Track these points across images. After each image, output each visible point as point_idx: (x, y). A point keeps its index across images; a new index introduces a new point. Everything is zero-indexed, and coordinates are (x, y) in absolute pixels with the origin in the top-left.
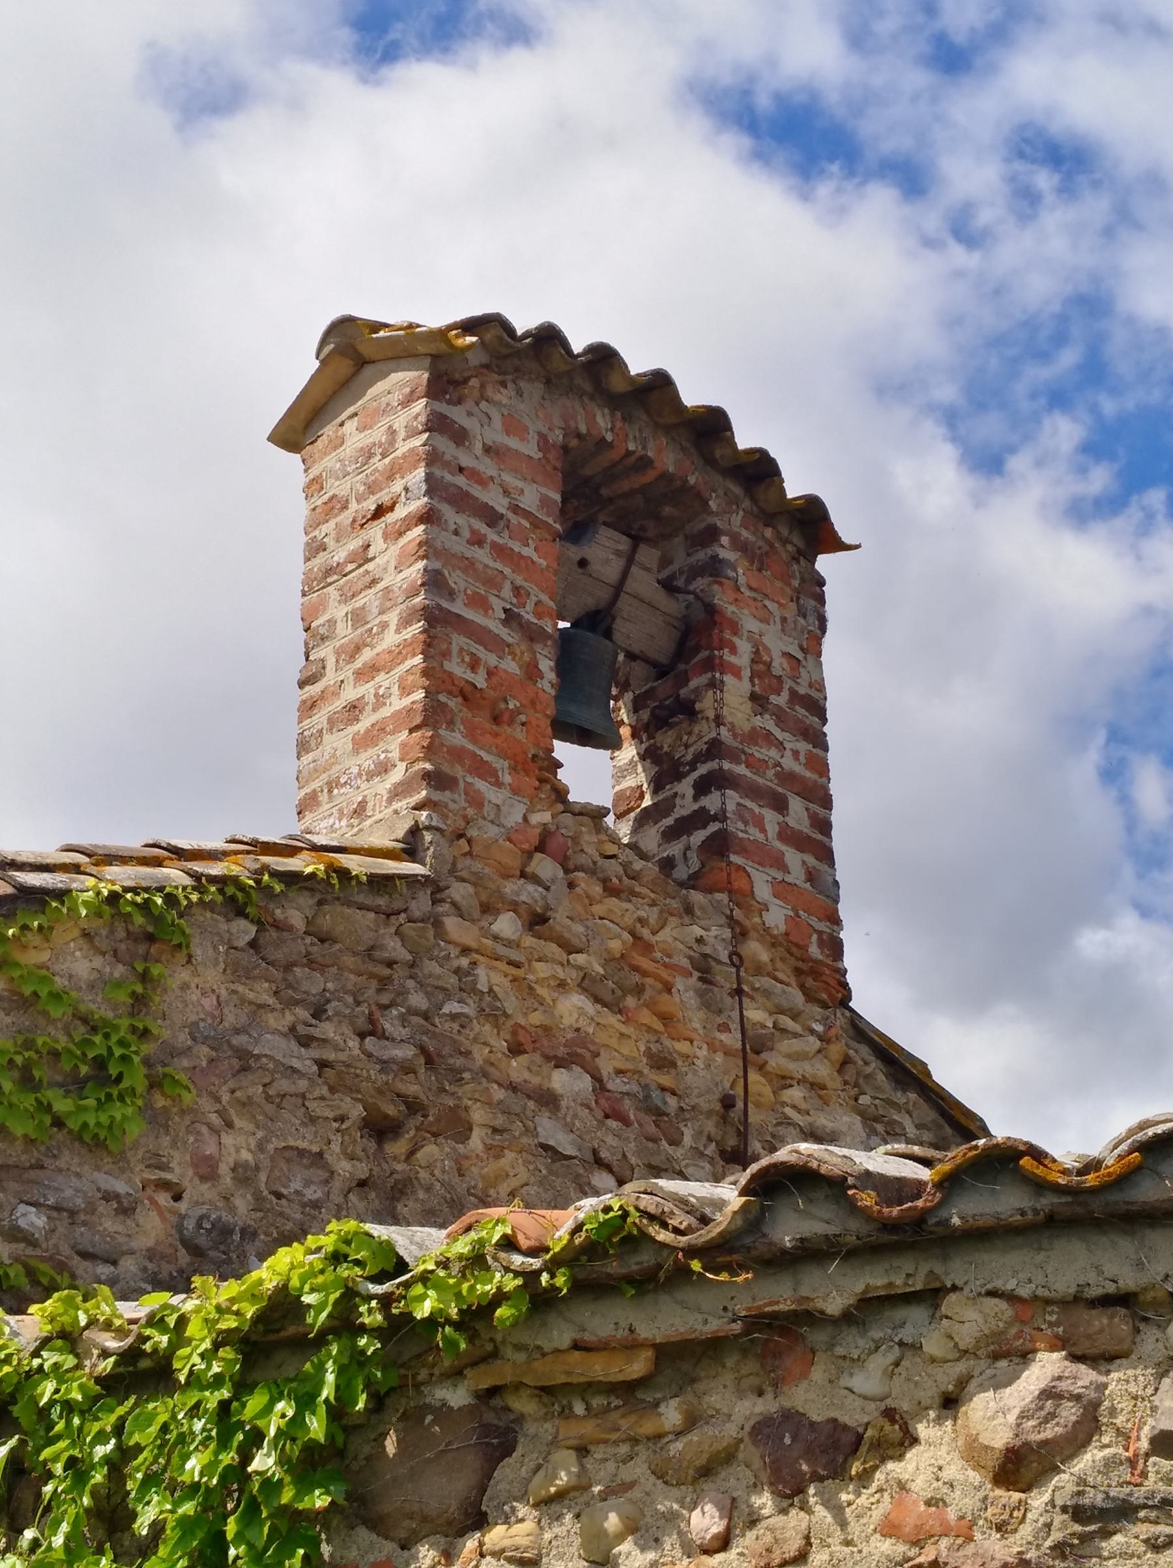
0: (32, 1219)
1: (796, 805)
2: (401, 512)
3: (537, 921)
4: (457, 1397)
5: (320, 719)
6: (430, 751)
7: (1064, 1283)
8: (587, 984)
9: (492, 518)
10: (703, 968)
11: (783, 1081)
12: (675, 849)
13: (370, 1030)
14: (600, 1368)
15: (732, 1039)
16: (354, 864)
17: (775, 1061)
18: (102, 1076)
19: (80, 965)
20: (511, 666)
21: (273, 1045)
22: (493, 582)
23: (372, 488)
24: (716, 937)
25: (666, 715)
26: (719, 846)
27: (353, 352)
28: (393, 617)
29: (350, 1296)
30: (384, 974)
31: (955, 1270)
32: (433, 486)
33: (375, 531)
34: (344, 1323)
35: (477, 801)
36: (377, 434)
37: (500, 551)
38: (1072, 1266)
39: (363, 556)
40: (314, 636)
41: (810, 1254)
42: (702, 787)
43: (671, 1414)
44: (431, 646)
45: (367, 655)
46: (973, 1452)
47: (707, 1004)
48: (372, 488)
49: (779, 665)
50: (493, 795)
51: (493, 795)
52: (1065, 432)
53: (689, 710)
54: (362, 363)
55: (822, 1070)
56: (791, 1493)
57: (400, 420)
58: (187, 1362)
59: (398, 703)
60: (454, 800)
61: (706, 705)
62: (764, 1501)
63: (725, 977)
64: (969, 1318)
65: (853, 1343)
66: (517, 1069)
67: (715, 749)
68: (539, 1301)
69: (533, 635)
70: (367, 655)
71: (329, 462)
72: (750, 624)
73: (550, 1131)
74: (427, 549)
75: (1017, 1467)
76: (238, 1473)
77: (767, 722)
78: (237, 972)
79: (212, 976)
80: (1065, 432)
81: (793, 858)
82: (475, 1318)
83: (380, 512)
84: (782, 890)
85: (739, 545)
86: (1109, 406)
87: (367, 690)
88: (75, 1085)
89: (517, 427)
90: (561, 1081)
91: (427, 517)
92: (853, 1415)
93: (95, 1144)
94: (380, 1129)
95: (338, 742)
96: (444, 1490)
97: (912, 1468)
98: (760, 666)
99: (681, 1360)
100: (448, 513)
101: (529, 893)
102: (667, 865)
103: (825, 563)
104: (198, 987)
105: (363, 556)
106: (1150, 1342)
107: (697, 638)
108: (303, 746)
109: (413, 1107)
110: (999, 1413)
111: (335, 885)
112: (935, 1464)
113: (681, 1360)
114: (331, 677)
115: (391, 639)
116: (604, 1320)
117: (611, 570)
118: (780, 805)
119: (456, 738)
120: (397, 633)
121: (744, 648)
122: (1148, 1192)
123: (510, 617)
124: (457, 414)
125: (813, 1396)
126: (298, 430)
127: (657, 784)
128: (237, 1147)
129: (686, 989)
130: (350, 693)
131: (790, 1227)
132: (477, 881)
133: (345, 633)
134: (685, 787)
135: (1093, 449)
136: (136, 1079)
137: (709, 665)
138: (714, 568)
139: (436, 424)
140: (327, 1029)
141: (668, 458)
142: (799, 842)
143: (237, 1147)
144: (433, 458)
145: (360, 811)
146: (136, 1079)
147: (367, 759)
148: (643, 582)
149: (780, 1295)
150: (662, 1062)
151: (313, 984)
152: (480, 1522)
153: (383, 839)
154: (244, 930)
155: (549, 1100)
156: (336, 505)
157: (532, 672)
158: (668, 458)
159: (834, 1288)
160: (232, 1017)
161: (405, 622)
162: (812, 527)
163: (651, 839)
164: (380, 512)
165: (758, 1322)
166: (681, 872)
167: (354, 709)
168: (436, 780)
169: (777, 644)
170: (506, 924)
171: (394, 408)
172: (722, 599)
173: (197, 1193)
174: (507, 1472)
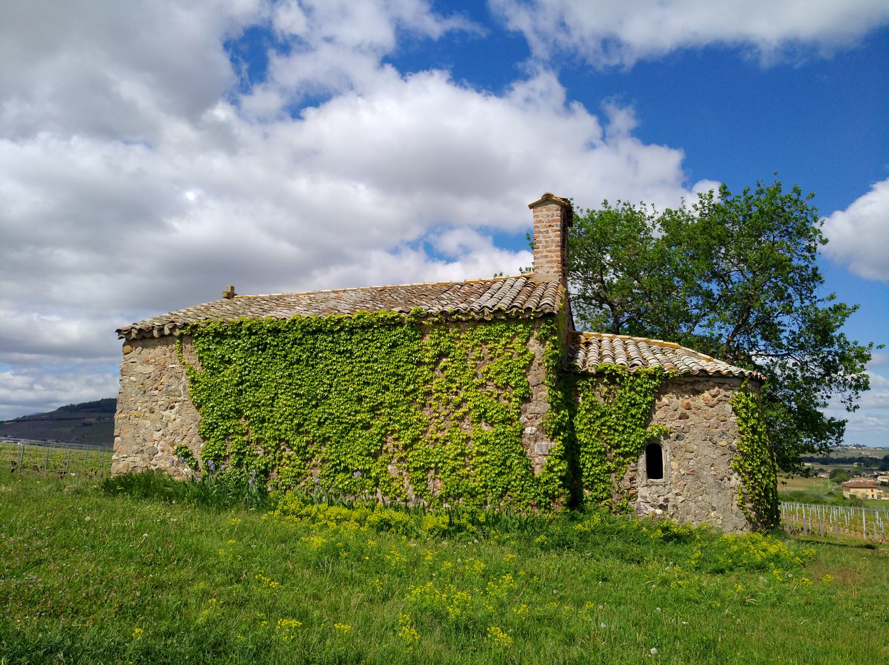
27: (547, 199)
33: (550, 229)
36: (550, 213)
64: (711, 383)
75: (714, 396)
87: (549, 254)
105: (547, 232)
112: (706, 394)
115: (553, 248)
125: (696, 387)
167: (546, 256)
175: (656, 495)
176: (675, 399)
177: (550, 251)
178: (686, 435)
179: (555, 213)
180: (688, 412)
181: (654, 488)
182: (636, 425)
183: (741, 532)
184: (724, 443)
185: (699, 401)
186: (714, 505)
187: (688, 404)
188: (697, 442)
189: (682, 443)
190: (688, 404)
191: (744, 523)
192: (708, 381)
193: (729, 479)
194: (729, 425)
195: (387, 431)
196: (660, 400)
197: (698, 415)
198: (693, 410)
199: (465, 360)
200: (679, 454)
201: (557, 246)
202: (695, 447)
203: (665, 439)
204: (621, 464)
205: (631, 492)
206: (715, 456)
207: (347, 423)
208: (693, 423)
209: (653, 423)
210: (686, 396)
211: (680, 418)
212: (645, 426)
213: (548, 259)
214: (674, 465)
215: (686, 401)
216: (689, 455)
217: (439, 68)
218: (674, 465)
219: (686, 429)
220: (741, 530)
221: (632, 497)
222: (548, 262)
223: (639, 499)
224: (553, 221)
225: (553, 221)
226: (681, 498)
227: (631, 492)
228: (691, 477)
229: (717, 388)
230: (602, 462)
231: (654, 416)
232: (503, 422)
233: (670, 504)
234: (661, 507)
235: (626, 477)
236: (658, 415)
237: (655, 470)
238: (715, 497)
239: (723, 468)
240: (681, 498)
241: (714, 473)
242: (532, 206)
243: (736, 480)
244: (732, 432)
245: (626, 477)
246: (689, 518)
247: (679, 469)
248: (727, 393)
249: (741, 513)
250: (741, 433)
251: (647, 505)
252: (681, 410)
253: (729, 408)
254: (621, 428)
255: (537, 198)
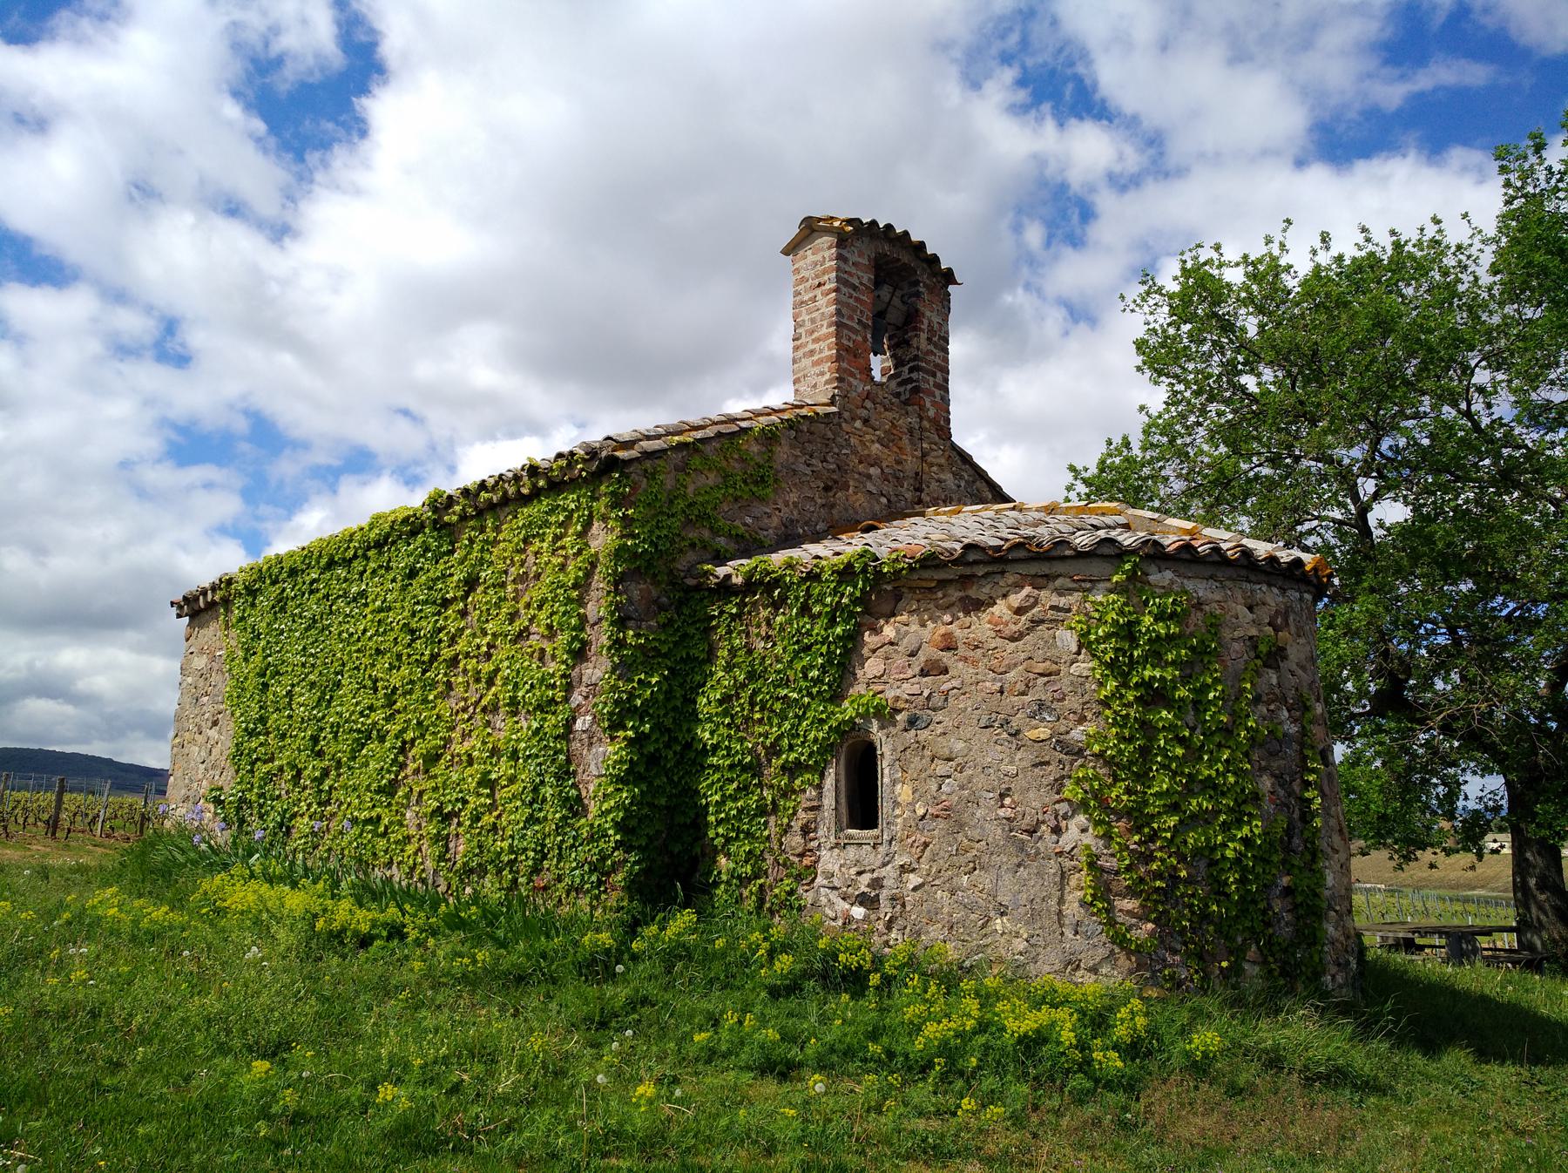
0: (749, 520)
1: (939, 374)
2: (827, 287)
3: (866, 421)
4: (889, 588)
5: (800, 353)
6: (838, 371)
7: (1033, 572)
8: (880, 441)
9: (855, 288)
10: (911, 431)
11: (932, 465)
12: (901, 389)
13: (824, 460)
14: (924, 584)
15: (918, 453)
16: (819, 410)
17: (929, 459)
18: (762, 481)
19: (755, 448)
20: (860, 338)
21: (802, 468)
22: (854, 311)
23: (817, 276)
24: (913, 420)
25: (900, 347)
26: (916, 390)
27: (811, 228)
28: (825, 323)
29: (866, 565)
30: (827, 443)
31: (1008, 568)
32: (838, 279)
33: (818, 292)
34: (864, 570)
35: (850, 385)
36: (818, 257)
37: (857, 299)
38: (1034, 568)
39: (814, 299)
40: (798, 325)
41: (976, 562)
42: (911, 370)
43: (940, 594)
44: (838, 335)
45: (816, 335)
46: (1010, 607)
47: (912, 443)
48: (817, 276)
49: (936, 326)
50: (855, 382)
51: (855, 382)
52: (1009, 75)
53: (907, 343)
54: (813, 231)
55: (943, 461)
56: (967, 613)
57: (827, 254)
58: (825, 577)
59: (827, 353)
60: (844, 386)
61: (914, 342)
62: (961, 615)
63: (917, 434)
64: (1011, 579)
65: (983, 582)
66: (861, 468)
67: (916, 358)
68: (911, 568)
69: (865, 326)
70: (816, 335)
71: (801, 263)
72: (928, 314)
73: (870, 487)
74: (837, 301)
75: (1019, 611)
76: (839, 603)
77: (931, 347)
78: (792, 447)
79: (786, 449)
80: (1009, 75)
81: (937, 393)
82: (897, 572)
83: (819, 285)
84: (934, 404)
85: (925, 286)
86: (1030, 62)
87: (816, 346)
88: (756, 483)
89: (861, 254)
90: (874, 471)
91: (837, 290)
92: (982, 597)
93: (762, 500)
94: (827, 489)
95: (807, 362)
96: (886, 608)
97: (995, 609)
98: (931, 330)
99: (943, 584)
100: (844, 290)
101: (864, 413)
102: (898, 395)
103: (951, 288)
104: (783, 452)
105: (814, 299)
106: (1051, 585)
107: (912, 318)
108: (794, 361)
109: (836, 482)
110: (1016, 599)
111: (815, 419)
112: (1000, 609)
113: (943, 584)
114: (803, 340)
115: (824, 330)
116: (927, 574)
117: (887, 299)
118: (934, 375)
119: (845, 365)
120: (826, 329)
121: (926, 322)
122: (1054, 553)
123: (860, 322)
124: (844, 252)
125: (973, 593)
126: (792, 249)
127: (896, 367)
128: (793, 497)
129: (906, 439)
130: (811, 346)
131: (971, 557)
132: (850, 411)
133: (808, 325)
134: (906, 369)
135: (1021, 83)
136: (771, 481)
137: (915, 329)
138: (918, 295)
139: (840, 257)
140: (814, 461)
141: (905, 258)
142: (937, 386)
143: (793, 497)
144: (838, 269)
145: (815, 386)
146: (771, 481)
147: (817, 370)
148: (896, 301)
149: (968, 571)
150: (899, 462)
151: (809, 447)
152: (894, 615)
153: (826, 400)
154: (793, 433)
155: (869, 477)
156: (804, 280)
157: (865, 339)
158: (905, 258)
159: (980, 571)
160: (791, 460)
161: (830, 326)
162: (949, 277)
163: (893, 384)
164: (819, 285)
165: (961, 576)
166: (903, 398)
167: (812, 352)
168: (840, 380)
169: (936, 319)
170: (858, 424)
171: (823, 251)
172: (920, 306)
173: (784, 509)
174: (901, 604)
175: (853, 871)
176: (914, 627)
177: (816, 341)
178: (939, 717)
179: (827, 254)
180: (947, 658)
181: (851, 852)
182: (810, 694)
183: (1090, 978)
184: (1043, 732)
185: (980, 626)
186: (1005, 900)
187: (947, 636)
188: (967, 732)
189: (924, 735)
190: (947, 636)
191: (1102, 952)
192: (1003, 573)
193: (1057, 830)
194: (1064, 684)
195: (404, 743)
196: (876, 631)
197: (975, 663)
198: (962, 650)
199: (503, 585)
200: (916, 763)
201: (830, 326)
202: (961, 745)
203: (882, 728)
204: (786, 793)
205: (807, 861)
206: (1012, 769)
207: (359, 731)
208: (955, 683)
209: (858, 689)
210: (947, 618)
211: (924, 673)
212: (836, 697)
213: (815, 358)
214: (904, 792)
215: (943, 630)
216: (941, 768)
217: (1466, 142)
218: (904, 792)
219: (937, 700)
220: (1094, 970)
221: (807, 875)
222: (815, 364)
223: (820, 880)
224: (824, 272)
225: (824, 272)
226: (914, 880)
227: (807, 861)
228: (942, 824)
229: (1027, 590)
230: (744, 789)
231: (859, 673)
232: (539, 707)
233: (884, 895)
234: (863, 900)
235: (796, 826)
236: (873, 667)
237: (863, 807)
238: (1007, 877)
239: (1034, 801)
240: (914, 880)
241: (1009, 813)
242: (787, 251)
243: (1078, 833)
244: (1073, 702)
245: (796, 826)
246: (935, 933)
247: (912, 804)
248: (1062, 602)
249: (1093, 924)
250: (1105, 703)
251: (833, 896)
252: (928, 652)
253: (1067, 639)
254: (778, 706)
255: (793, 231)
